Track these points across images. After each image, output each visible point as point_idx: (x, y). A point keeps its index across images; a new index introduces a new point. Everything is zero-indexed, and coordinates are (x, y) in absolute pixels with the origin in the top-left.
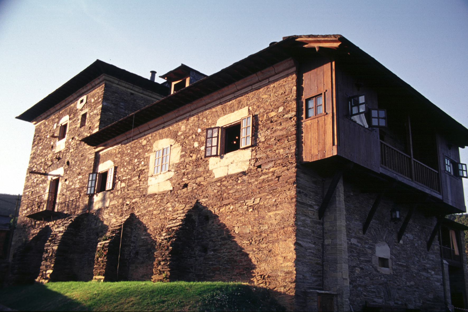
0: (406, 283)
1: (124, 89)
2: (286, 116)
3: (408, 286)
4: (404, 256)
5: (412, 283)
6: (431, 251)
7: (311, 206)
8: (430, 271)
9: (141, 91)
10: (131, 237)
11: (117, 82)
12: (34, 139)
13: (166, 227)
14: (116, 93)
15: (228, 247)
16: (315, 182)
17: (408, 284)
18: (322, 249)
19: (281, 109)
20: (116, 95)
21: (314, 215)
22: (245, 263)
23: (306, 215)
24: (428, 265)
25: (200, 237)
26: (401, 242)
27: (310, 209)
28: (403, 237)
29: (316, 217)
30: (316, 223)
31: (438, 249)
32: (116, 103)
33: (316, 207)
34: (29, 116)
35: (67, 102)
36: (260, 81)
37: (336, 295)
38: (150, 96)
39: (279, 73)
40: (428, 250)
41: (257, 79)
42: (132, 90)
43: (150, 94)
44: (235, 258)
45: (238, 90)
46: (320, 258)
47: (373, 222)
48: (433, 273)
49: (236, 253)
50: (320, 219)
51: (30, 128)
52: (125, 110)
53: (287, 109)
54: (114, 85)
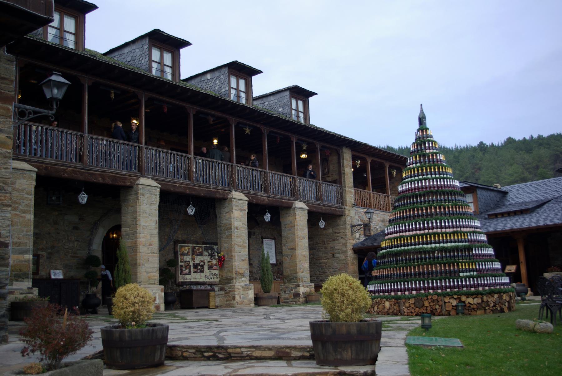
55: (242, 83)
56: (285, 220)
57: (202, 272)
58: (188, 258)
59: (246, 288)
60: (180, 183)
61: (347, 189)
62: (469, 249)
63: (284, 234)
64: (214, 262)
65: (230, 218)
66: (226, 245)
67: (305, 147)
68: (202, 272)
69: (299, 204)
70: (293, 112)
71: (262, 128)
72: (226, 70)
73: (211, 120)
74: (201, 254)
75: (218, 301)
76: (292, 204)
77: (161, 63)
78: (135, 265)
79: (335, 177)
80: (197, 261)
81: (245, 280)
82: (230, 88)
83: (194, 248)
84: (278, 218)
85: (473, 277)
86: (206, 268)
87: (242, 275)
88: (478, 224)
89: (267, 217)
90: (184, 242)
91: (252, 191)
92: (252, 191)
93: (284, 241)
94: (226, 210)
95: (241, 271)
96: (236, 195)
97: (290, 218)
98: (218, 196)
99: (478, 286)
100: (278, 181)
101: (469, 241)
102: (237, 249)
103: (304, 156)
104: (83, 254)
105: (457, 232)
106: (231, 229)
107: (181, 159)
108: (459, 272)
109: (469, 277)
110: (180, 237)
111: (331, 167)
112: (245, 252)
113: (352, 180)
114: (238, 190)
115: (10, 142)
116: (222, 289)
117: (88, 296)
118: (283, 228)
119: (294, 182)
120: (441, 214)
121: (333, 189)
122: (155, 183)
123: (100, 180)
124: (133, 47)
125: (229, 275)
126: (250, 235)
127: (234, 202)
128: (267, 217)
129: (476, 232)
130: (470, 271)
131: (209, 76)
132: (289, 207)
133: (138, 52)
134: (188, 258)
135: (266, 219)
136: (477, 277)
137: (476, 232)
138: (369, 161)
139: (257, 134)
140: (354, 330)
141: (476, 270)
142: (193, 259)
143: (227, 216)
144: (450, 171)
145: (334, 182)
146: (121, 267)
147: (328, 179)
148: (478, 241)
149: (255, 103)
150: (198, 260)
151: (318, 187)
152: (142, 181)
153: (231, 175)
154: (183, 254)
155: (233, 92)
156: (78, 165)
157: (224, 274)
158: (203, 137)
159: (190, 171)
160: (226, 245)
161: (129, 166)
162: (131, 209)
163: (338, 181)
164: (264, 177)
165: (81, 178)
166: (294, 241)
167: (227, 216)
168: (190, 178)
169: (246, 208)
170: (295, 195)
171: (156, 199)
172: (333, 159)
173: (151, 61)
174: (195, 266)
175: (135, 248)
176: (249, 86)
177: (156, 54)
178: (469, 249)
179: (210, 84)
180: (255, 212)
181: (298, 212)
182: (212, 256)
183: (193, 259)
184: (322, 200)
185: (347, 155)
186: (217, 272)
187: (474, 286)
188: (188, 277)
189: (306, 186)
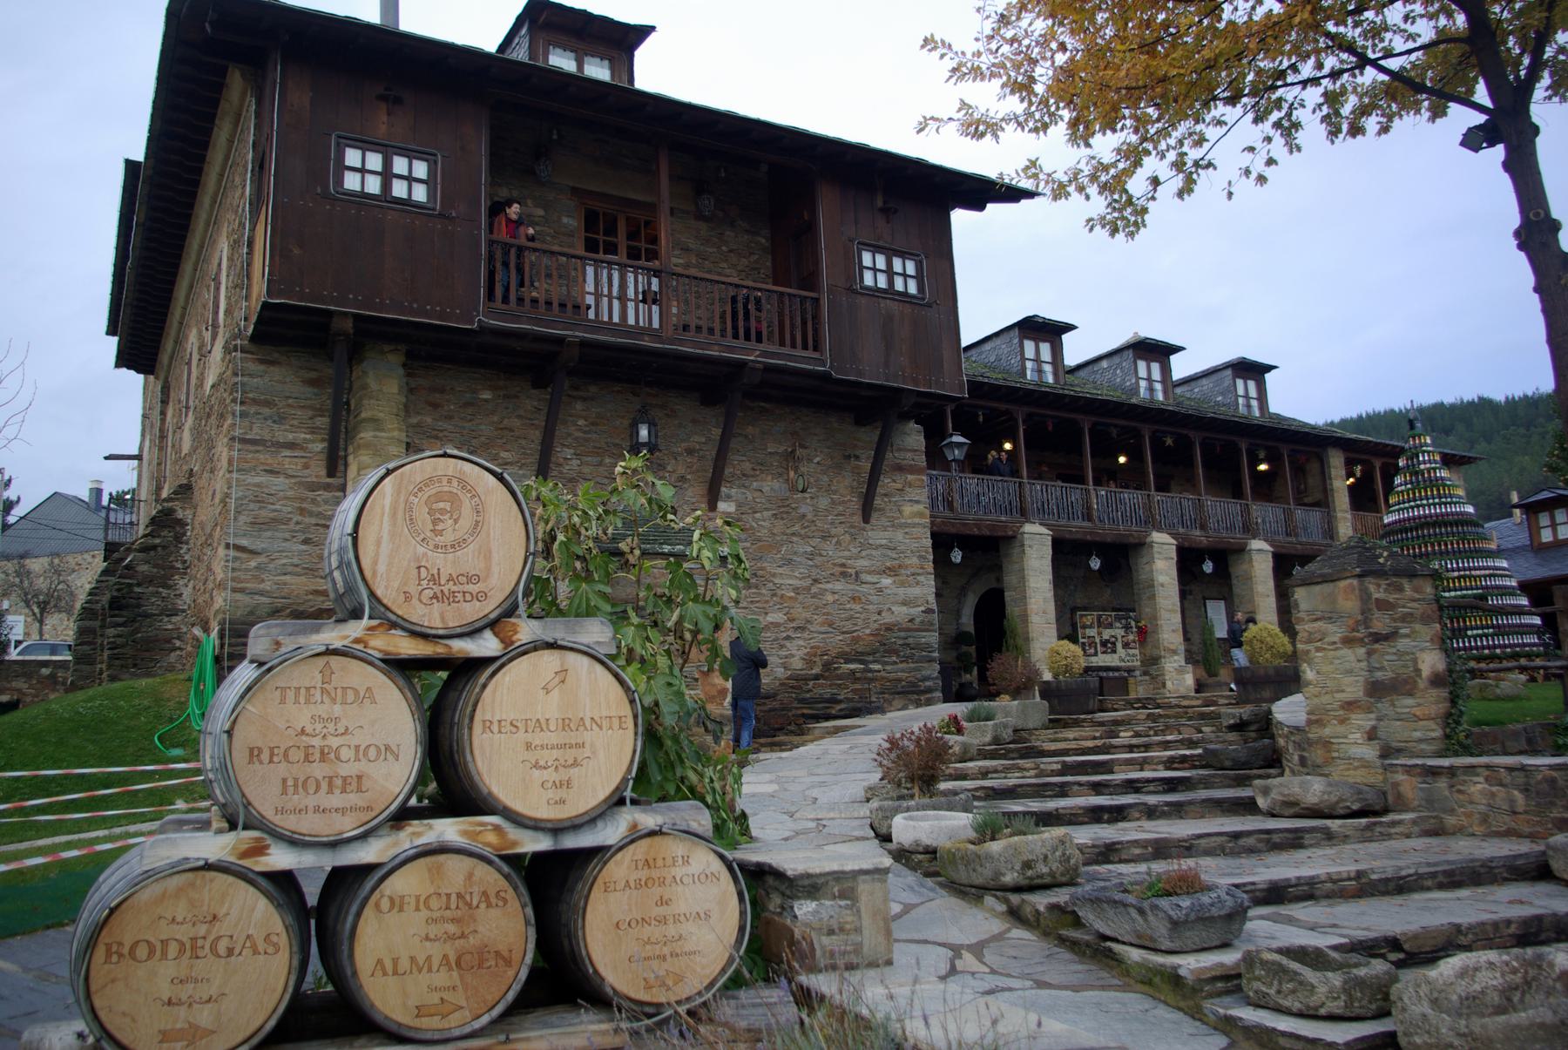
7: (291, 446)
8: (869, 578)
16: (312, 383)
21: (306, 467)
26: (722, 506)
27: (288, 453)
29: (318, 471)
33: (319, 446)
40: (866, 519)
50: (331, 474)
55: (1155, 367)
56: (1237, 570)
57: (1114, 652)
58: (1092, 632)
59: (1180, 671)
60: (1077, 527)
61: (1339, 515)
62: (1483, 598)
63: (1236, 590)
64: (1131, 637)
67: (1262, 455)
68: (1114, 652)
69: (1257, 544)
70: (1241, 401)
71: (1191, 434)
72: (1130, 353)
73: (1114, 432)
74: (1110, 626)
77: (1037, 360)
78: (1027, 639)
79: (1318, 496)
80: (1106, 637)
81: (1180, 659)
82: (1138, 378)
83: (1099, 617)
84: (1227, 567)
85: (1486, 636)
86: (1119, 645)
87: (1174, 652)
88: (1505, 564)
89: (1208, 567)
90: (1085, 609)
91: (1181, 530)
92: (1181, 530)
93: (1236, 601)
94: (1145, 560)
96: (1158, 537)
97: (1245, 567)
98: (1131, 540)
99: (1495, 647)
100: (1219, 510)
101: (1482, 588)
102: (1164, 614)
103: (1263, 467)
104: (951, 630)
105: (1464, 577)
107: (1075, 494)
108: (1467, 629)
109: (1481, 636)
110: (1079, 602)
111: (1311, 481)
112: (1177, 619)
113: (1347, 499)
114: (1160, 530)
115: (927, 512)
116: (1145, 673)
117: (962, 685)
118: (1234, 582)
119: (1246, 511)
120: (1441, 553)
121: (1314, 517)
122: (1044, 530)
123: (976, 531)
124: (998, 342)
125: (1155, 652)
126: (1183, 595)
128: (1208, 567)
129: (1494, 576)
130: (1482, 628)
131: (1105, 364)
132: (1241, 550)
133: (1005, 349)
134: (1092, 632)
135: (1208, 569)
136: (1492, 636)
137: (1494, 576)
138: (1377, 464)
139: (1184, 445)
140: (1271, 672)
141: (1493, 627)
142: (1100, 634)
143: (1147, 568)
144: (1461, 492)
145: (1316, 504)
146: (1011, 642)
147: (1306, 500)
148: (1506, 587)
149: (1178, 391)
150: (1107, 634)
151: (1288, 515)
152: (1028, 528)
154: (1084, 627)
155: (1143, 384)
156: (948, 513)
157: (1148, 652)
158: (1105, 451)
159: (1089, 508)
161: (1008, 510)
162: (1016, 566)
163: (1324, 502)
164: (1199, 506)
165: (953, 530)
166: (1252, 601)
167: (1147, 568)
168: (1089, 518)
169: (1174, 555)
170: (1250, 530)
171: (1048, 551)
172: (1314, 467)
173: (1023, 359)
174: (1104, 644)
175: (1025, 618)
176: (1166, 370)
177: (1029, 347)
178: (1483, 598)
179: (1108, 375)
180: (1188, 560)
181: (1255, 557)
182: (1127, 628)
183: (1100, 634)
184: (1296, 535)
185: (1336, 461)
186: (1136, 652)
187: (1488, 647)
188: (1094, 659)
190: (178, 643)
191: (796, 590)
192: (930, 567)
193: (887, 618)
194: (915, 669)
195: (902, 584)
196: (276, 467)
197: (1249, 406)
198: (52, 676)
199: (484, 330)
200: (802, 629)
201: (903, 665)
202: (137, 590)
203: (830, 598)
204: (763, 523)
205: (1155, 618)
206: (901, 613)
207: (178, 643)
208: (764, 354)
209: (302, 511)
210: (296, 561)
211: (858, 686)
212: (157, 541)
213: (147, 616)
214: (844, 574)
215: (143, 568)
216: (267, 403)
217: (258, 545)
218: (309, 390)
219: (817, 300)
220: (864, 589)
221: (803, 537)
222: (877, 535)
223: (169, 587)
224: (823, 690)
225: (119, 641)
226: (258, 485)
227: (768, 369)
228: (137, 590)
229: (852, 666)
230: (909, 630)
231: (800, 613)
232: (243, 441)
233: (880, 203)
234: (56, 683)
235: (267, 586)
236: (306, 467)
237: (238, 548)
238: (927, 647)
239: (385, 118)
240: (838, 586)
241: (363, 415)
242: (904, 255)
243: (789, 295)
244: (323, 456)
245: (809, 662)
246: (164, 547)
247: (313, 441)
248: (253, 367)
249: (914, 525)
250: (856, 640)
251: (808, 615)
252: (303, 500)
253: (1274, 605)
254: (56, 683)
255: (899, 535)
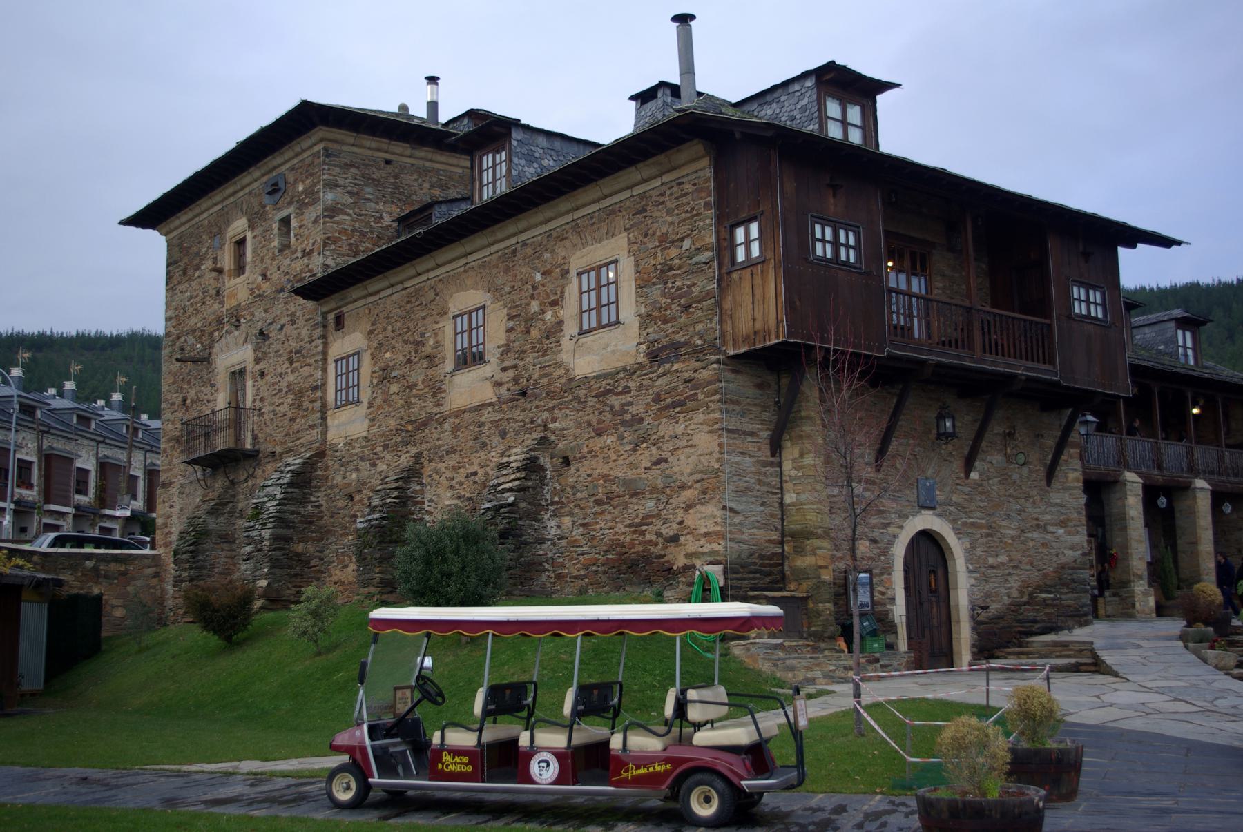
0: (986, 560)
1: (369, 153)
2: (697, 259)
3: (992, 567)
4: (981, 504)
5: (1003, 558)
6: (1056, 484)
7: (752, 434)
8: (1051, 529)
9: (408, 152)
10: (423, 503)
11: (351, 140)
12: (168, 273)
13: (490, 484)
14: (352, 166)
15: (609, 517)
16: (759, 386)
17: (991, 561)
18: (779, 512)
19: (687, 244)
20: (353, 170)
21: (759, 449)
22: (640, 548)
23: (742, 453)
24: (1048, 517)
25: (556, 499)
26: (974, 475)
27: (750, 439)
28: (977, 463)
29: (765, 454)
30: (765, 464)
31: (1077, 480)
32: (355, 190)
33: (765, 434)
34: (147, 218)
35: (239, 187)
36: (646, 181)
37: (807, 598)
38: (431, 161)
39: (679, 167)
40: (1049, 483)
41: (639, 177)
42: (386, 152)
43: (429, 156)
44: (622, 538)
45: (606, 197)
46: (777, 529)
47: (893, 446)
48: (1061, 531)
49: (623, 530)
50: (773, 455)
51: (154, 244)
52: (377, 203)
53: (698, 245)
54: (345, 148)
56: (1181, 505)
59: (1146, 594)
65: (1124, 506)
66: (1118, 540)
70: (1181, 350)
75: (1110, 610)
76: (1190, 483)
87: (1140, 577)
91: (1144, 470)
93: (1179, 532)
95: (1139, 573)
98: (1110, 479)
100: (1173, 452)
102: (1134, 544)
106: (1125, 519)
114: (1130, 470)
119: (1157, 449)
127: (1129, 486)
153: (1121, 449)
160: (1118, 540)
169: (1140, 492)
180: (1150, 493)
181: (1200, 495)
189: (1139, 446)
190: (547, 566)
191: (1013, 538)
192: (1084, 519)
193: (1062, 560)
194: (1079, 598)
195: (1069, 533)
196: (745, 450)
197: (1186, 355)
198: (95, 569)
199: (891, 357)
200: (1016, 567)
201: (1070, 595)
202: (520, 523)
203: (1031, 544)
204: (994, 485)
205: (1127, 548)
206: (1070, 555)
207: (547, 566)
208: (1027, 369)
209: (760, 482)
210: (758, 518)
211: (1047, 611)
212: (530, 483)
213: (527, 544)
214: (1038, 526)
215: (523, 505)
216: (738, 403)
217: (739, 507)
218: (758, 392)
219: (1050, 326)
220: (1049, 537)
221: (1016, 498)
222: (1055, 496)
223: (538, 520)
224: (1028, 613)
225: (512, 564)
226: (737, 463)
227: (1029, 379)
228: (520, 523)
229: (1044, 595)
230: (1073, 568)
231: (1016, 556)
232: (729, 431)
233: (1081, 249)
234: (98, 576)
235: (745, 537)
236: (759, 449)
237: (731, 510)
238: (1083, 582)
239: (832, 200)
240: (1035, 535)
241: (803, 414)
242: (1095, 288)
243: (1037, 323)
244: (768, 441)
245: (1021, 593)
246: (534, 488)
247: (761, 430)
248: (731, 376)
249: (1075, 488)
250: (1045, 576)
251: (1019, 557)
252: (760, 473)
253: (1211, 538)
254: (98, 576)
255: (1066, 496)
